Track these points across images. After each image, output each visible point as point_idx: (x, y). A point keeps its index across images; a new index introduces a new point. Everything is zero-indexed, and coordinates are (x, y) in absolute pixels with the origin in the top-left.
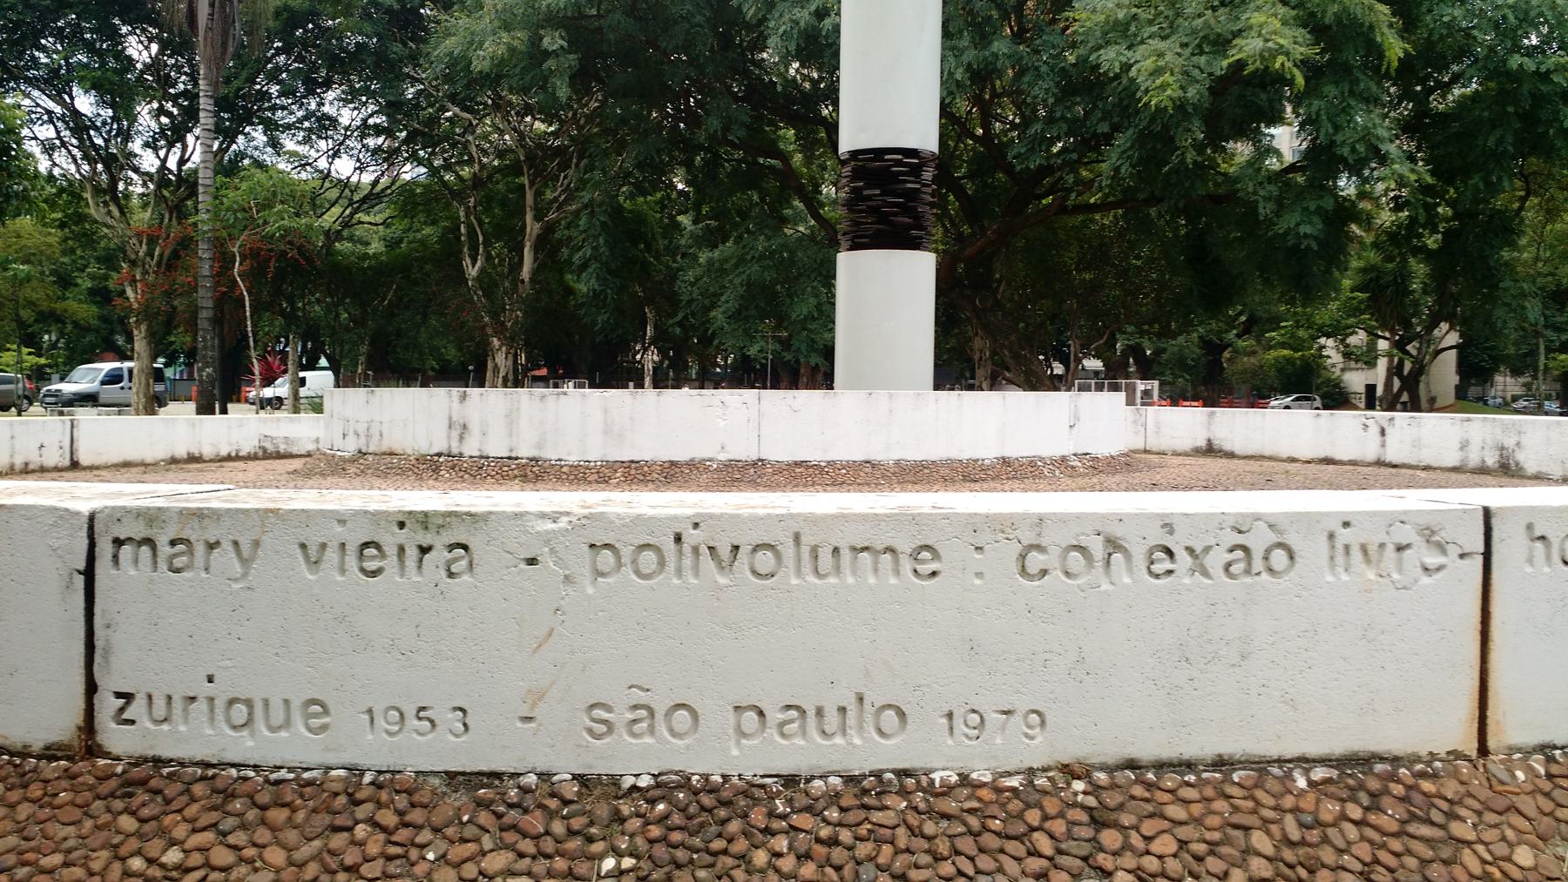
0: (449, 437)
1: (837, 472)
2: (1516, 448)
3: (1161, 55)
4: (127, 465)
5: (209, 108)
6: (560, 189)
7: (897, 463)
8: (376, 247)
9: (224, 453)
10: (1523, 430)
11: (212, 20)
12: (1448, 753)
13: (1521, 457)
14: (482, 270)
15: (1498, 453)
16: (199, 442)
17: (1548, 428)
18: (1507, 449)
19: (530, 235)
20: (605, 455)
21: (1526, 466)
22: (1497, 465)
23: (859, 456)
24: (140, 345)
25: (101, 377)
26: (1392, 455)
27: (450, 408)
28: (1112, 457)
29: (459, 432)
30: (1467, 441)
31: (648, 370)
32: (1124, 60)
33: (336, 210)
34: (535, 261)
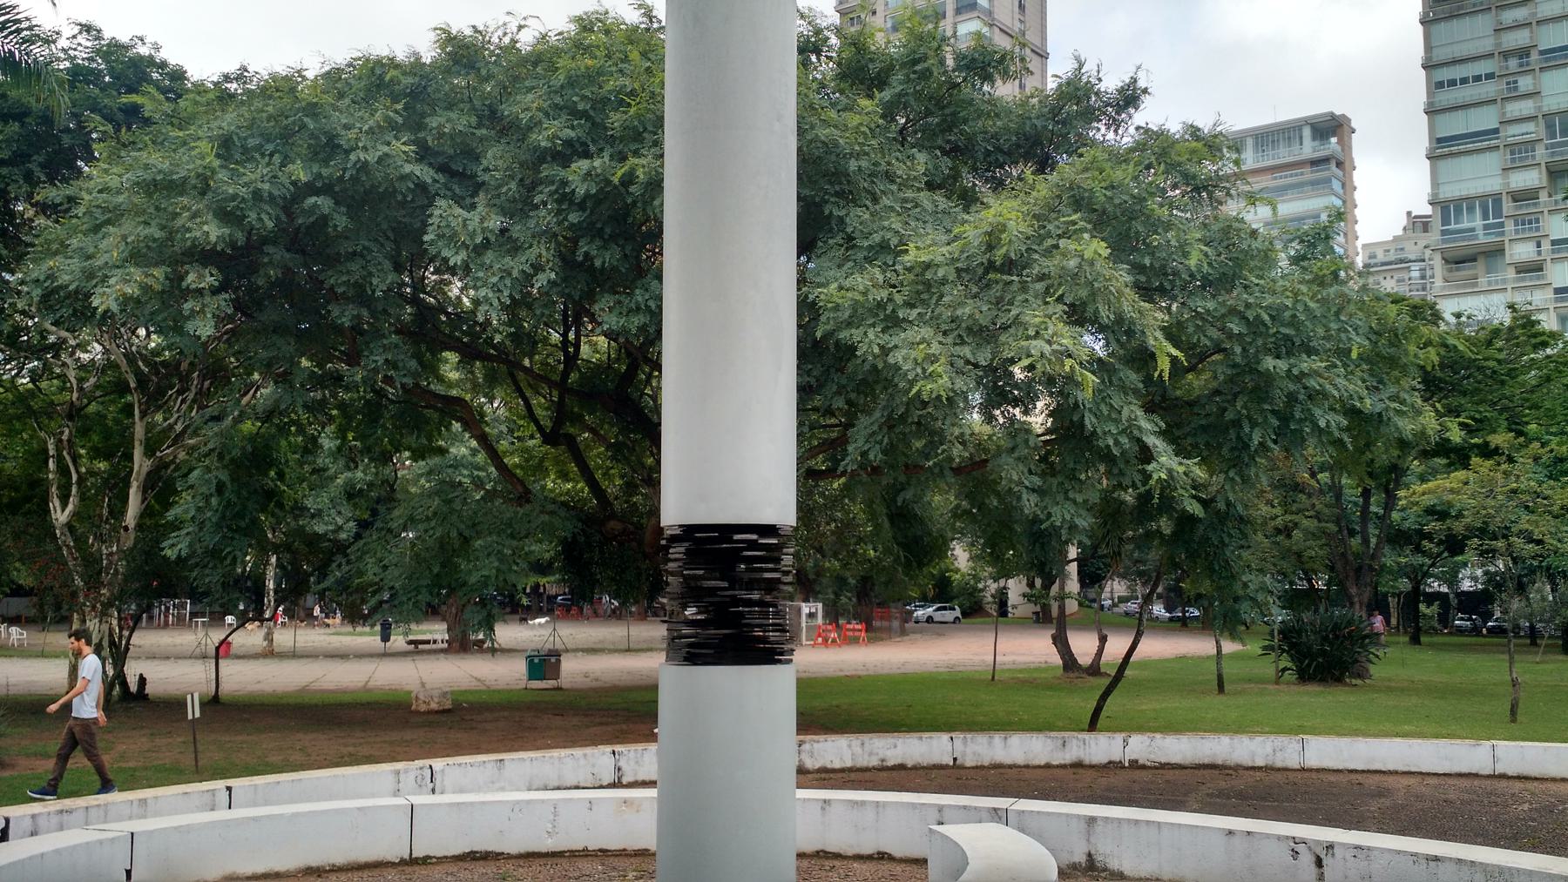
6: (176, 416)
14: (75, 514)
34: (143, 502)
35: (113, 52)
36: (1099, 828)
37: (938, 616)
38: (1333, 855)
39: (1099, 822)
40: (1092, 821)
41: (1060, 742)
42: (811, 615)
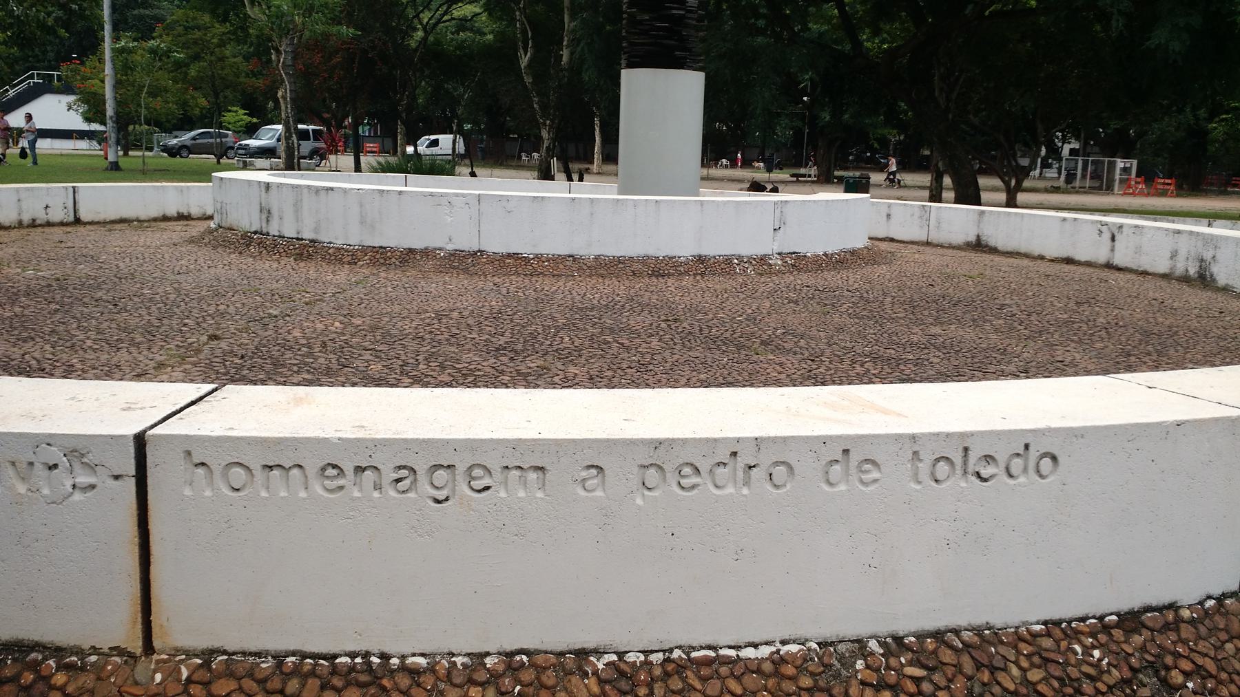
0: (261, 219)
1: (540, 263)
2: (1212, 262)
4: (122, 221)
7: (597, 258)
10: (1218, 245)
12: (110, 648)
15: (1198, 264)
16: (188, 205)
17: (702, 205)
20: (361, 241)
21: (1218, 278)
22: (1196, 275)
26: (1119, 260)
28: (825, 254)
30: (1176, 251)
36: (986, 218)
38: (1122, 232)
39: (987, 214)
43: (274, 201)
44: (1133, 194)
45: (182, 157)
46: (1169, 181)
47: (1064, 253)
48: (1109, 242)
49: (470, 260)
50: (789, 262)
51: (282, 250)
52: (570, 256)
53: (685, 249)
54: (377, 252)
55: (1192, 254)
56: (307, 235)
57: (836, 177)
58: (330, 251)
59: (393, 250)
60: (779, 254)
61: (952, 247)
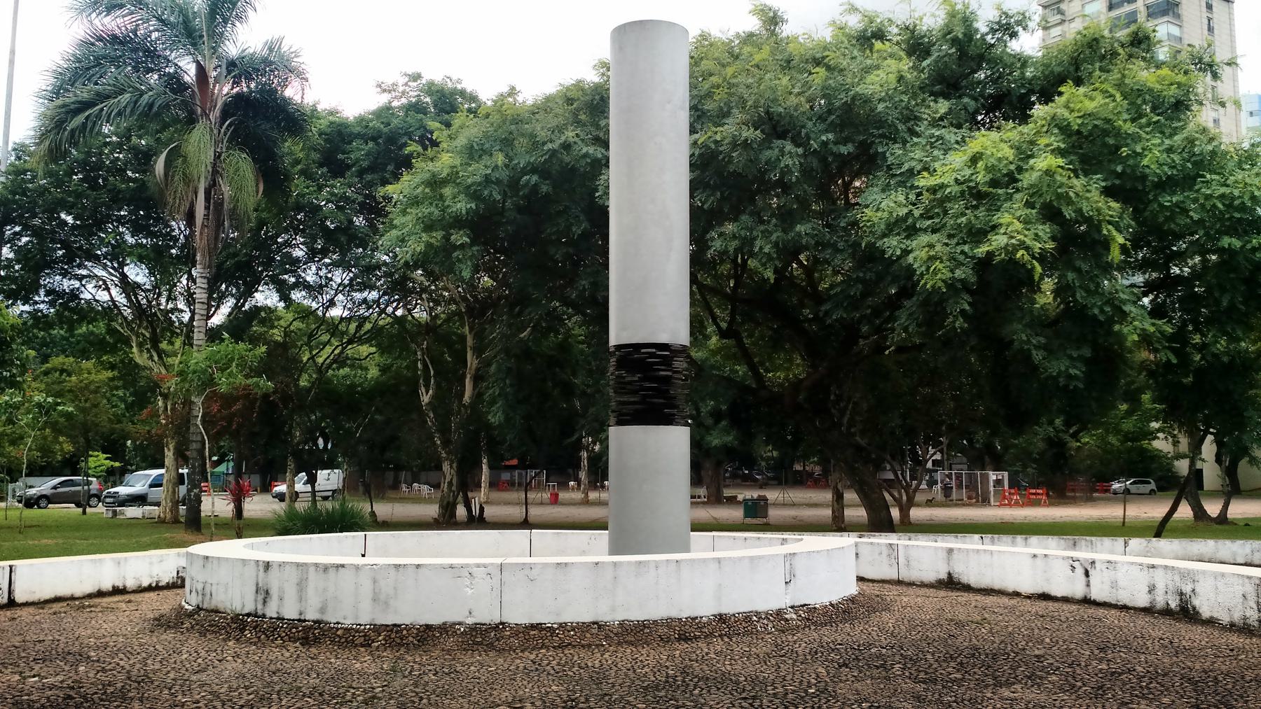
0: (256, 601)
1: (566, 633)
2: (1192, 595)
3: (931, 246)
5: (203, 286)
7: (622, 624)
8: (373, 372)
9: (145, 584)
10: (1196, 579)
11: (208, 219)
13: (1196, 602)
14: (433, 397)
15: (1178, 598)
16: (124, 577)
18: (1186, 595)
19: (470, 369)
20: (373, 619)
21: (1201, 611)
22: (1178, 608)
23: (587, 618)
24: (169, 456)
25: (149, 482)
26: (1097, 593)
27: (257, 576)
28: (831, 605)
29: (263, 596)
30: (1154, 586)
31: (584, 466)
32: (904, 247)
33: (328, 349)
35: (431, 89)
36: (955, 555)
37: (1133, 489)
40: (950, 551)
41: (1072, 542)
42: (998, 482)
43: (274, 581)
44: (1010, 505)
45: (39, 507)
46: (1040, 491)
47: (1039, 589)
48: (1083, 578)
49: (492, 634)
50: (803, 615)
51: (284, 634)
52: (594, 623)
53: (705, 608)
54: (392, 631)
55: (1170, 587)
56: (311, 615)
57: (725, 498)
58: (339, 633)
59: (408, 628)
60: (792, 607)
61: (923, 585)
